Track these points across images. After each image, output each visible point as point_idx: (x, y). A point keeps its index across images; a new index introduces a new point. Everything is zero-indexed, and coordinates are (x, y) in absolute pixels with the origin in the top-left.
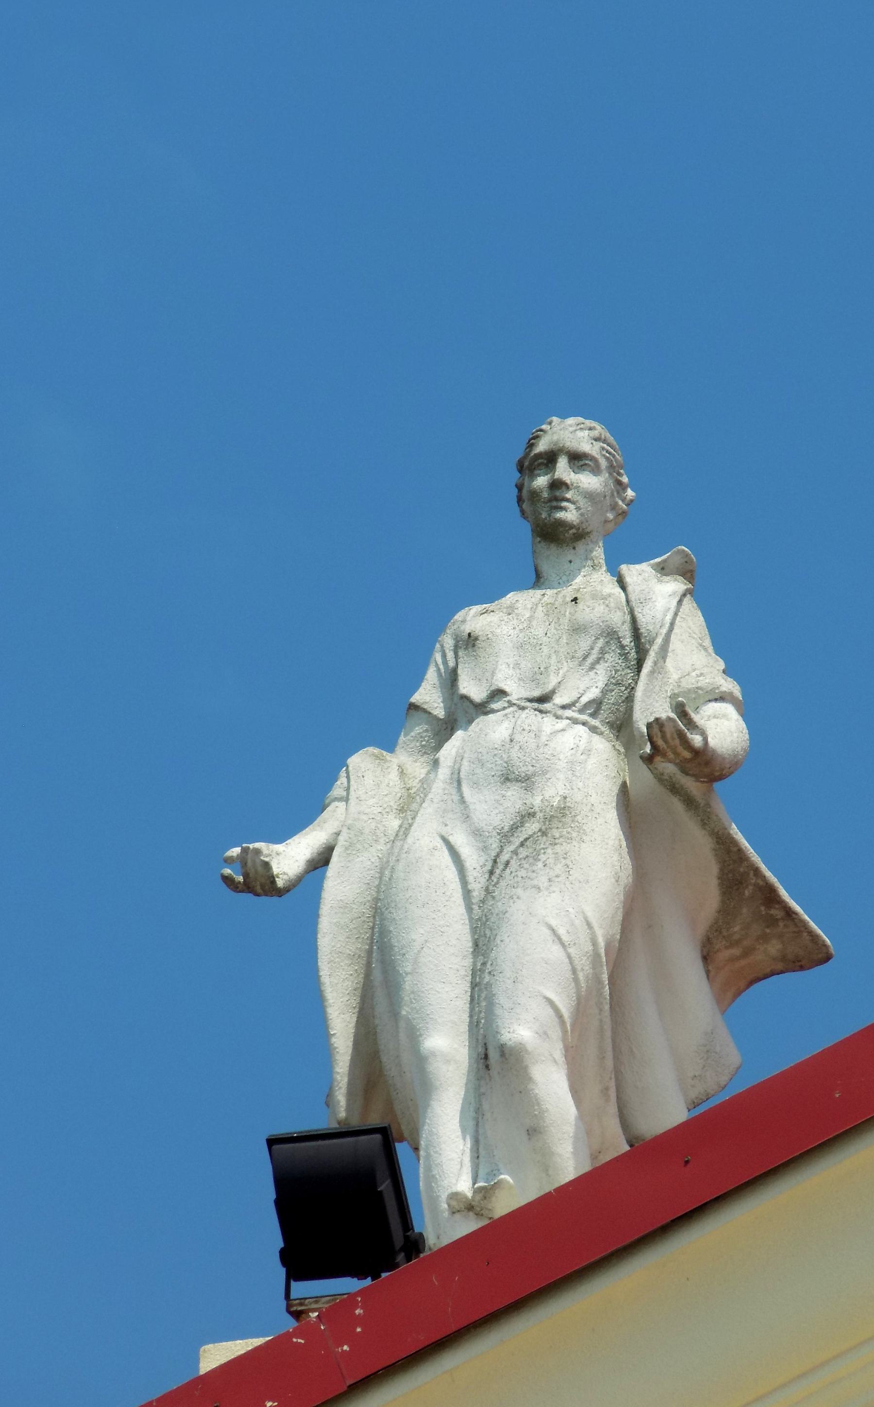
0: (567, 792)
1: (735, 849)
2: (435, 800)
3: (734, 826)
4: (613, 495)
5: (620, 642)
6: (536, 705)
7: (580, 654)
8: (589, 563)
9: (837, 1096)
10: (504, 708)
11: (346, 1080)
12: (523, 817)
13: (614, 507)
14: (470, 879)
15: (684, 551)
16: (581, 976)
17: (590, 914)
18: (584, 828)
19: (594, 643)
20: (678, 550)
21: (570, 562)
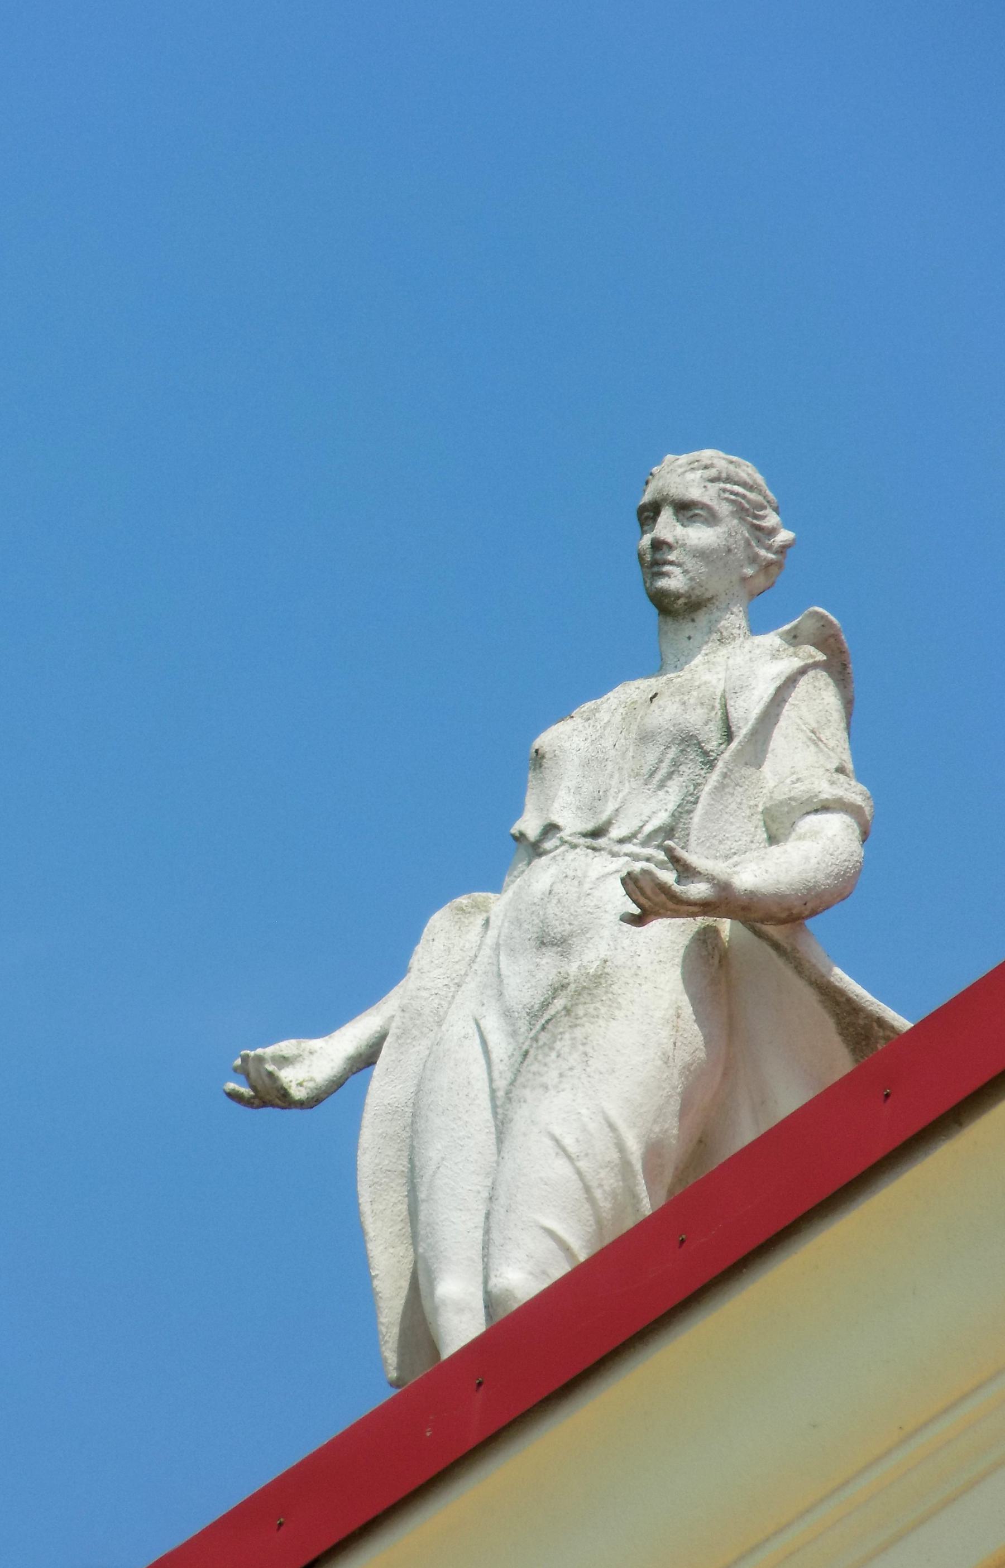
0: (609, 953)
1: (844, 999)
2: (479, 972)
3: (837, 971)
4: (748, 544)
5: (702, 748)
6: (589, 841)
7: (645, 770)
8: (715, 636)
9: (428, 1434)
10: (557, 847)
11: (395, 1330)
12: (555, 990)
13: (754, 559)
14: (496, 1075)
15: (817, 613)
16: (598, 1194)
17: (615, 1114)
18: (620, 1000)
19: (664, 753)
20: (811, 613)
21: (689, 638)
